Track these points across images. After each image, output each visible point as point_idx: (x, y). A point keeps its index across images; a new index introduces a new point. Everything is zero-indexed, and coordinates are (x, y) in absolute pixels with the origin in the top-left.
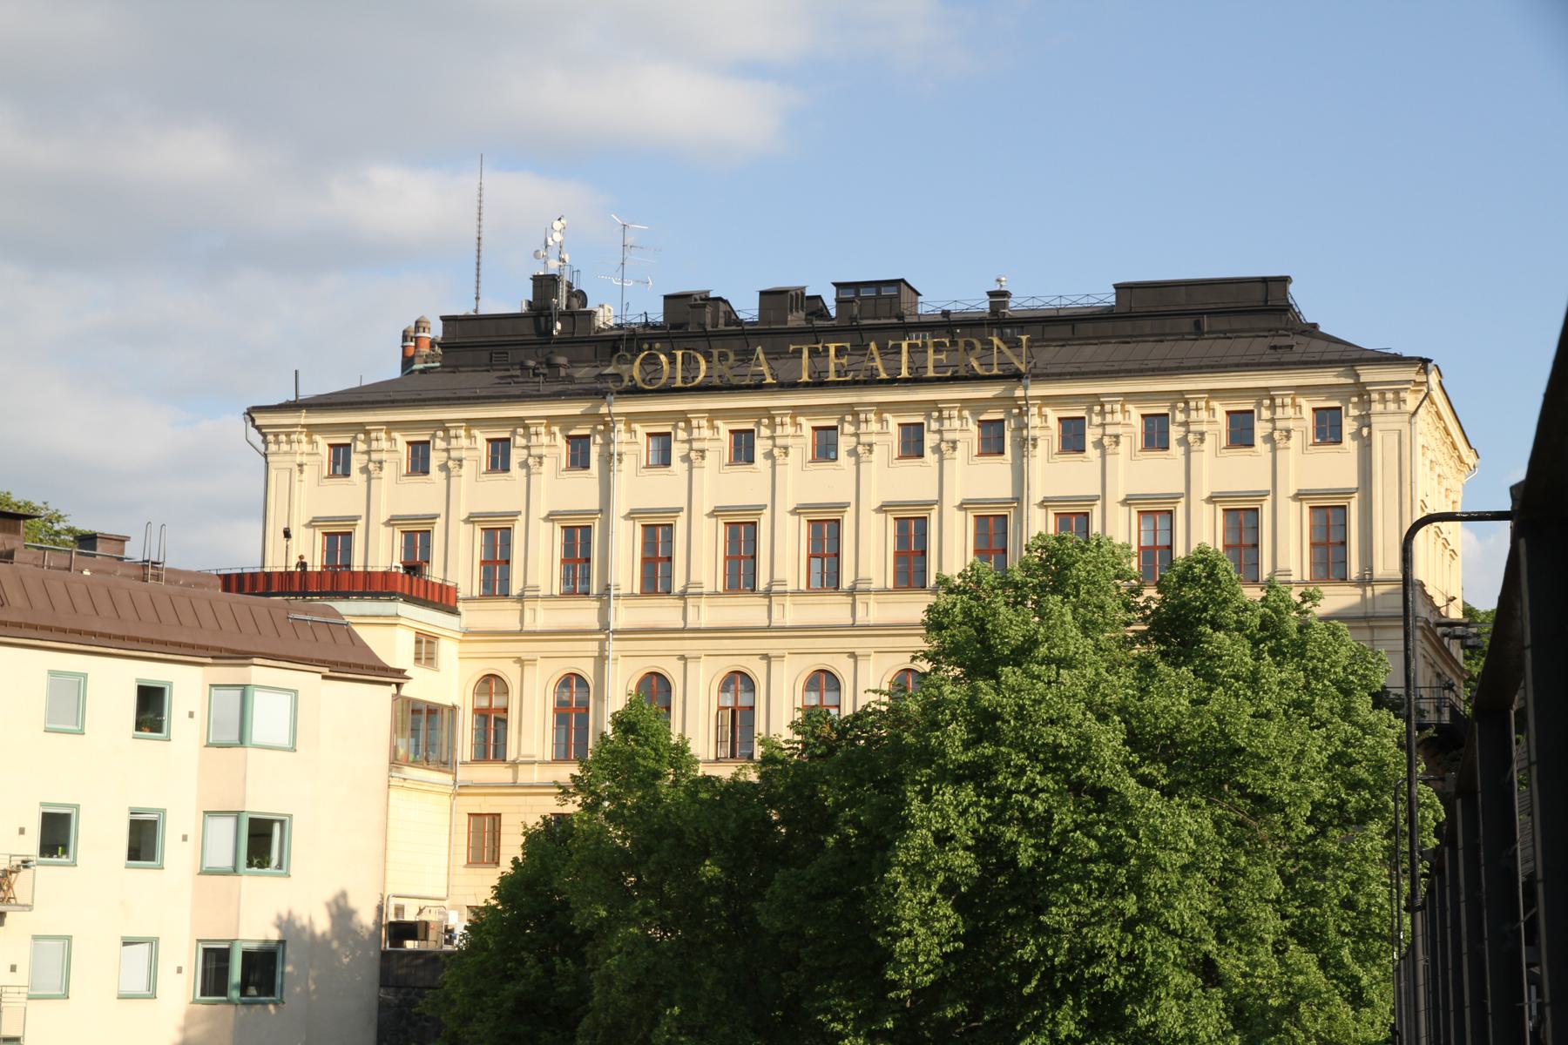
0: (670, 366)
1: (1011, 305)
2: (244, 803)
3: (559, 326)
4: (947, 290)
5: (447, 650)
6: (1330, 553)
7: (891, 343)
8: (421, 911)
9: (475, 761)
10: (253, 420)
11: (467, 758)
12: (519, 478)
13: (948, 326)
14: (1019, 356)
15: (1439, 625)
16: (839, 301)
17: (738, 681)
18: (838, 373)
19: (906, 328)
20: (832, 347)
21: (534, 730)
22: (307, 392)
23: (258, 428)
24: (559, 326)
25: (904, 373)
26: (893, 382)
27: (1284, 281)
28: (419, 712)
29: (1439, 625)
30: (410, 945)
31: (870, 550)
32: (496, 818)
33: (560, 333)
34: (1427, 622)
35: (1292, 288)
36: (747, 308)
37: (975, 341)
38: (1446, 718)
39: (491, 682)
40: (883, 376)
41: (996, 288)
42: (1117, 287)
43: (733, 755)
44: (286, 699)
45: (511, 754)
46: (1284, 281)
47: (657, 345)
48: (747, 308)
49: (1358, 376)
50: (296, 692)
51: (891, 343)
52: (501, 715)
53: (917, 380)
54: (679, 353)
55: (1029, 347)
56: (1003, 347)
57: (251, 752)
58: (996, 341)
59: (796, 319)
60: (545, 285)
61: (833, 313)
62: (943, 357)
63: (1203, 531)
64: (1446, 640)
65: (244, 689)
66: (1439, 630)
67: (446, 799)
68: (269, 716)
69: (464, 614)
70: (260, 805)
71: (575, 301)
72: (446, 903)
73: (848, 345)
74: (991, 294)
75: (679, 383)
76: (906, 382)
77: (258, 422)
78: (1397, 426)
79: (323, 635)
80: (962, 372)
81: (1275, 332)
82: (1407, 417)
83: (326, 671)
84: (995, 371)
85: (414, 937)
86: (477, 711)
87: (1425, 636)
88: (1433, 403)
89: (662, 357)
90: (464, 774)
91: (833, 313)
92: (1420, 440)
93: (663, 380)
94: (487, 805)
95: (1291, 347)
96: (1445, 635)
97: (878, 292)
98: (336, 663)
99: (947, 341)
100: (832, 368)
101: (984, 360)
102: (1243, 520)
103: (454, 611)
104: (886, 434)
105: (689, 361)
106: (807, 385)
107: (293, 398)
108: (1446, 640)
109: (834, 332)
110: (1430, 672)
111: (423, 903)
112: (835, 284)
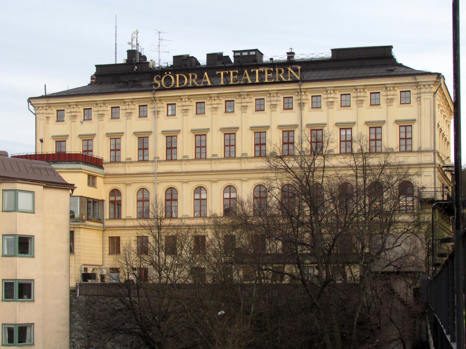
0: (175, 81)
1: (295, 57)
2: (16, 232)
3: (136, 67)
4: (273, 52)
5: (99, 181)
6: (406, 140)
7: (252, 70)
8: (93, 270)
9: (110, 219)
10: (30, 102)
11: (108, 218)
12: (124, 123)
13: (273, 65)
14: (298, 75)
15: (443, 167)
16: (235, 57)
17: (199, 190)
18: (233, 81)
19: (258, 66)
20: (231, 72)
21: (130, 208)
22: (49, 92)
23: (32, 105)
24: (136, 67)
25: (257, 81)
26: (254, 84)
27: (391, 47)
28: (90, 202)
29: (443, 167)
30: (90, 281)
31: (245, 143)
32: (118, 238)
33: (137, 70)
34: (439, 165)
35: (393, 50)
36: (203, 61)
37: (282, 69)
38: (445, 198)
39: (115, 192)
40: (250, 82)
41: (290, 51)
42: (332, 50)
43: (200, 216)
44: (30, 195)
45: (123, 216)
46: (391, 47)
47: (170, 73)
48: (203, 61)
49: (416, 79)
50: (34, 192)
51: (252, 70)
52: (119, 203)
53: (262, 83)
54: (178, 76)
55: (301, 71)
56: (292, 71)
57: (18, 214)
58: (289, 69)
59: (219, 64)
60: (131, 53)
61: (233, 61)
62: (271, 75)
63: (361, 131)
64: (446, 172)
65: (16, 191)
66: (444, 169)
67: (101, 232)
68: (24, 201)
69: (105, 168)
70: (23, 231)
71: (142, 59)
72: (102, 267)
73: (237, 71)
74: (288, 53)
75: (178, 86)
76: (257, 84)
77: (32, 103)
78: (429, 97)
79: (44, 172)
80: (277, 80)
81: (386, 65)
82: (432, 94)
83: (45, 185)
84: (289, 80)
85: (91, 279)
86: (111, 202)
87: (439, 170)
88: (442, 89)
89: (172, 77)
90: (107, 223)
91: (233, 61)
92: (437, 103)
93: (172, 86)
94: (115, 234)
95: (393, 70)
96: (445, 171)
97: (249, 53)
98: (48, 182)
99: (272, 69)
100: (232, 79)
101: (286, 76)
102: (375, 127)
103: (102, 167)
104: (252, 103)
105: (182, 79)
106: (222, 86)
107: (44, 94)
108: (446, 172)
109: (233, 67)
110: (440, 183)
111: (94, 267)
112: (234, 51)
